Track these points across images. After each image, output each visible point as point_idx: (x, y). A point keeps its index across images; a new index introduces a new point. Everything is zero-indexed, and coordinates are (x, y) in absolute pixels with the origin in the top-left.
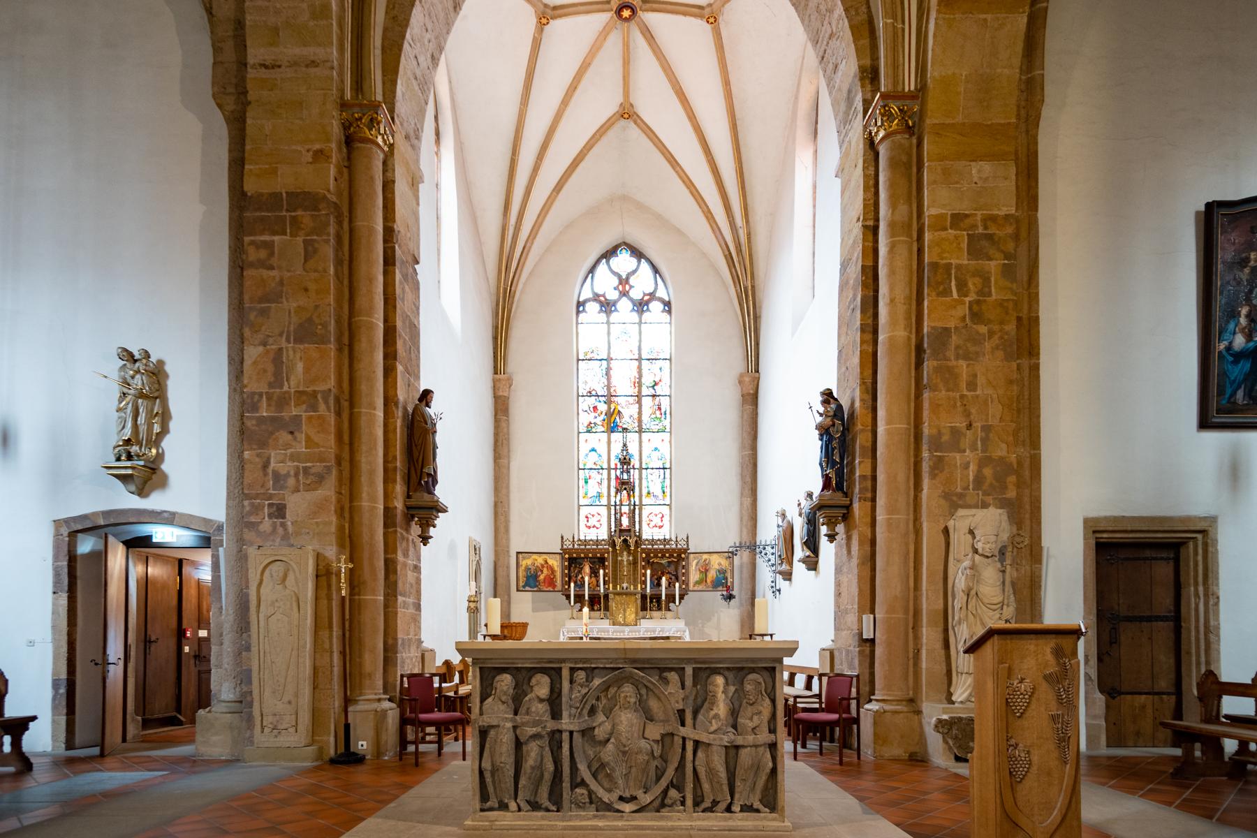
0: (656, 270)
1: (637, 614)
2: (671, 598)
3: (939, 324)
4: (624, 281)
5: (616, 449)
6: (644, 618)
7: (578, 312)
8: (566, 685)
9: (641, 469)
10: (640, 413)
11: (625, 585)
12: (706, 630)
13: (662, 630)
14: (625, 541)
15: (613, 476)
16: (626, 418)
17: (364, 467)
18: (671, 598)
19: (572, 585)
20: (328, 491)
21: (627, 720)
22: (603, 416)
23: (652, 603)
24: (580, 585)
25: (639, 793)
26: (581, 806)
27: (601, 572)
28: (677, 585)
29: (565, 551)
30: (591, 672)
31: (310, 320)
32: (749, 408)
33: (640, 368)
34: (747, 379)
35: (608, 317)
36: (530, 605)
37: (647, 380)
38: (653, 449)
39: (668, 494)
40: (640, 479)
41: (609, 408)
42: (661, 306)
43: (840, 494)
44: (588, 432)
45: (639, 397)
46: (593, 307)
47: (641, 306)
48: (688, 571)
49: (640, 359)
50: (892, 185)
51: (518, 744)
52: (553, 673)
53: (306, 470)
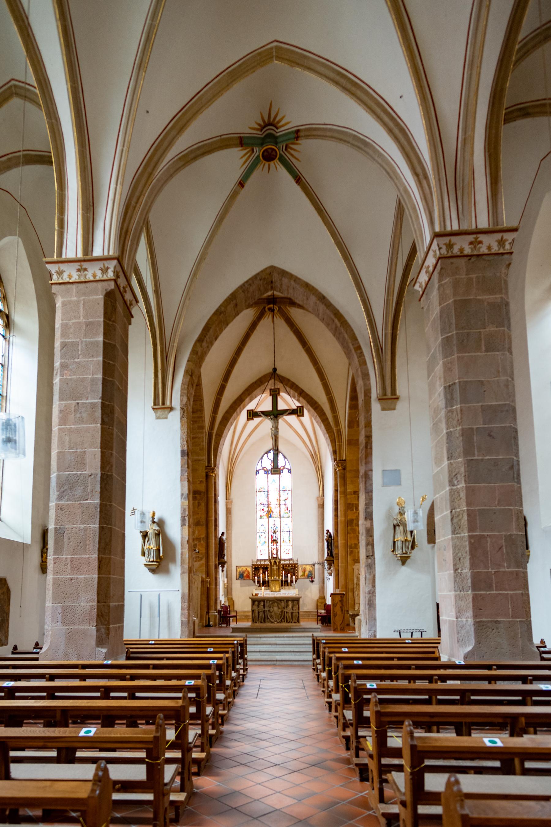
0: (285, 457)
2: (292, 581)
5: (271, 524)
7: (256, 474)
12: (306, 593)
14: (275, 561)
17: (211, 555)
18: (292, 581)
19: (256, 577)
20: (203, 561)
21: (276, 609)
22: (266, 512)
23: (285, 584)
27: (266, 573)
29: (253, 565)
30: (270, 601)
31: (199, 521)
32: (321, 509)
33: (280, 494)
34: (320, 499)
36: (239, 585)
37: (282, 499)
38: (287, 524)
46: (262, 472)
50: (340, 483)
51: (259, 613)
52: (264, 601)
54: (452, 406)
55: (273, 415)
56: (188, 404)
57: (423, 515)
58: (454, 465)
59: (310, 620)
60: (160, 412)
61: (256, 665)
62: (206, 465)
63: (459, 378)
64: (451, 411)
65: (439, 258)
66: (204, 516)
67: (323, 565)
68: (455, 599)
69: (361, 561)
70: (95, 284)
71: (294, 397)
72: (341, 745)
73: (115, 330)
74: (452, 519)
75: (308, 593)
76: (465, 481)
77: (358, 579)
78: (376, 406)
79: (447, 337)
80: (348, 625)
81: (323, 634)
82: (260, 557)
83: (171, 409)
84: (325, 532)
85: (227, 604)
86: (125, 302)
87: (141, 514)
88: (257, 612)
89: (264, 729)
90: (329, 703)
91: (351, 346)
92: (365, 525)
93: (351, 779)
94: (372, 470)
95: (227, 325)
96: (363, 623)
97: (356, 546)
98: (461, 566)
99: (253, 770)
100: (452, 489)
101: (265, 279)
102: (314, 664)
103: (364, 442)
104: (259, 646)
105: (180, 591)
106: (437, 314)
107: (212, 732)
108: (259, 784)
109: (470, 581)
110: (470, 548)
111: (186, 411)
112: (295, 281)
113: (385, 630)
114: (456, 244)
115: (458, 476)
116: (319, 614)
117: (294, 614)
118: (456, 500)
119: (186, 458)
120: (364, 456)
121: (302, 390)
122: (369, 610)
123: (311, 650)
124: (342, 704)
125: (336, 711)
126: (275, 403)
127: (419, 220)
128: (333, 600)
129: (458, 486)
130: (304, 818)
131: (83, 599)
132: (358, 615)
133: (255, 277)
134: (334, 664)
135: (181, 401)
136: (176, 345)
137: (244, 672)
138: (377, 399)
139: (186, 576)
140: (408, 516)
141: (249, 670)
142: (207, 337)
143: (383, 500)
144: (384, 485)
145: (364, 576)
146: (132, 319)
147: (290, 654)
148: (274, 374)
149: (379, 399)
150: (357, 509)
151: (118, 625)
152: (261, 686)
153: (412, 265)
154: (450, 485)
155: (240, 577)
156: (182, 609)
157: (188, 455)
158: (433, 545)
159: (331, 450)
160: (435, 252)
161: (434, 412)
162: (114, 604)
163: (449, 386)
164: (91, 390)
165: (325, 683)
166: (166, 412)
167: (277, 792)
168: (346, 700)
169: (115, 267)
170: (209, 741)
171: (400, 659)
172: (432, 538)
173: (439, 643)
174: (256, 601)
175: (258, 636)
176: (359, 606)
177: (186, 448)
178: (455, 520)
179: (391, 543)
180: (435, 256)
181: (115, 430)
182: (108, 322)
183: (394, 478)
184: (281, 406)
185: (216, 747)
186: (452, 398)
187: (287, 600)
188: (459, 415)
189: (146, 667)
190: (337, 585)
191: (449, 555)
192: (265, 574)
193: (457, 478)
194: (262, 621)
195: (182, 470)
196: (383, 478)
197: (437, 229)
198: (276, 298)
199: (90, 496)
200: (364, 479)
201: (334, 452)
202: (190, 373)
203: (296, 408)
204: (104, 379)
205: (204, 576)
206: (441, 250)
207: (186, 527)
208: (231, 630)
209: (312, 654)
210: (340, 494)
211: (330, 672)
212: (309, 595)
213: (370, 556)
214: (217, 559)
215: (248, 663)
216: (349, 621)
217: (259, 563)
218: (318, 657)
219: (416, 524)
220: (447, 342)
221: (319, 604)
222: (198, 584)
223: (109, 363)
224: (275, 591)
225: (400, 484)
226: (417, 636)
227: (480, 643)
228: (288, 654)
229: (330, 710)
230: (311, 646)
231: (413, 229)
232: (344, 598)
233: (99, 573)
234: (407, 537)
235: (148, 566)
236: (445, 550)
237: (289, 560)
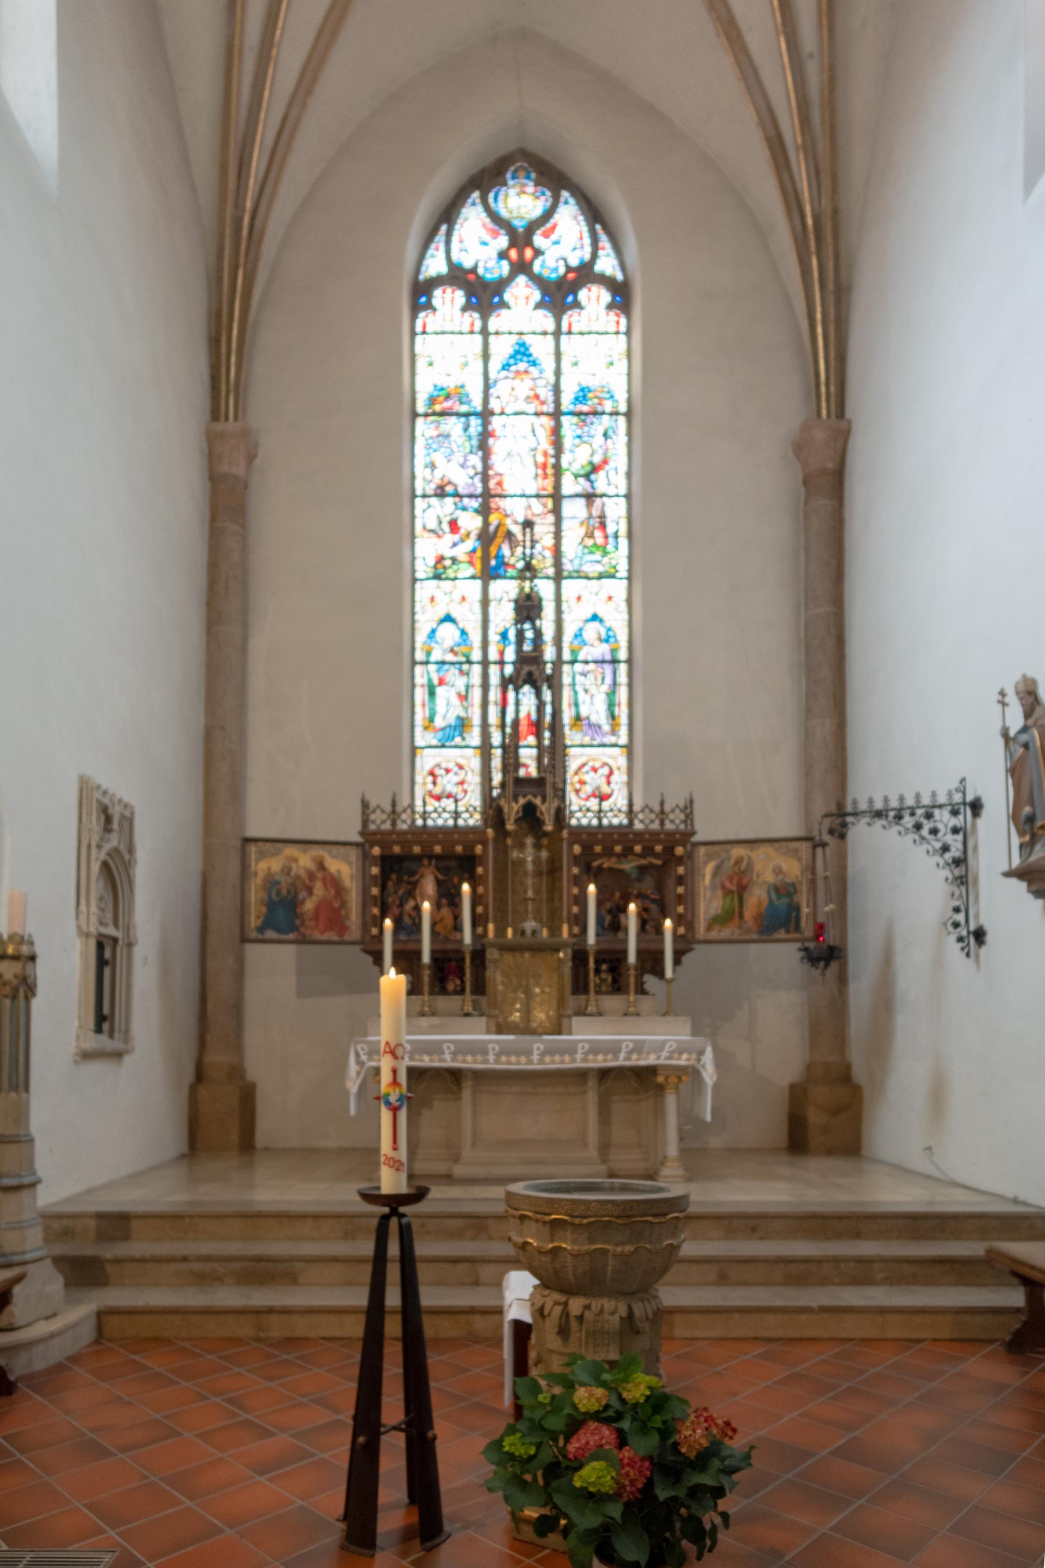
1: (561, 1003)
2: (651, 961)
4: (521, 238)
6: (581, 1013)
11: (530, 925)
14: (529, 810)
19: (388, 923)
22: (470, 544)
23: (604, 974)
27: (466, 887)
28: (668, 923)
32: (823, 503)
33: (556, 433)
37: (575, 458)
39: (624, 719)
41: (486, 523)
42: (606, 297)
44: (437, 577)
46: (449, 302)
47: (559, 295)
49: (557, 414)
155: (268, 923)
224: (525, 1029)
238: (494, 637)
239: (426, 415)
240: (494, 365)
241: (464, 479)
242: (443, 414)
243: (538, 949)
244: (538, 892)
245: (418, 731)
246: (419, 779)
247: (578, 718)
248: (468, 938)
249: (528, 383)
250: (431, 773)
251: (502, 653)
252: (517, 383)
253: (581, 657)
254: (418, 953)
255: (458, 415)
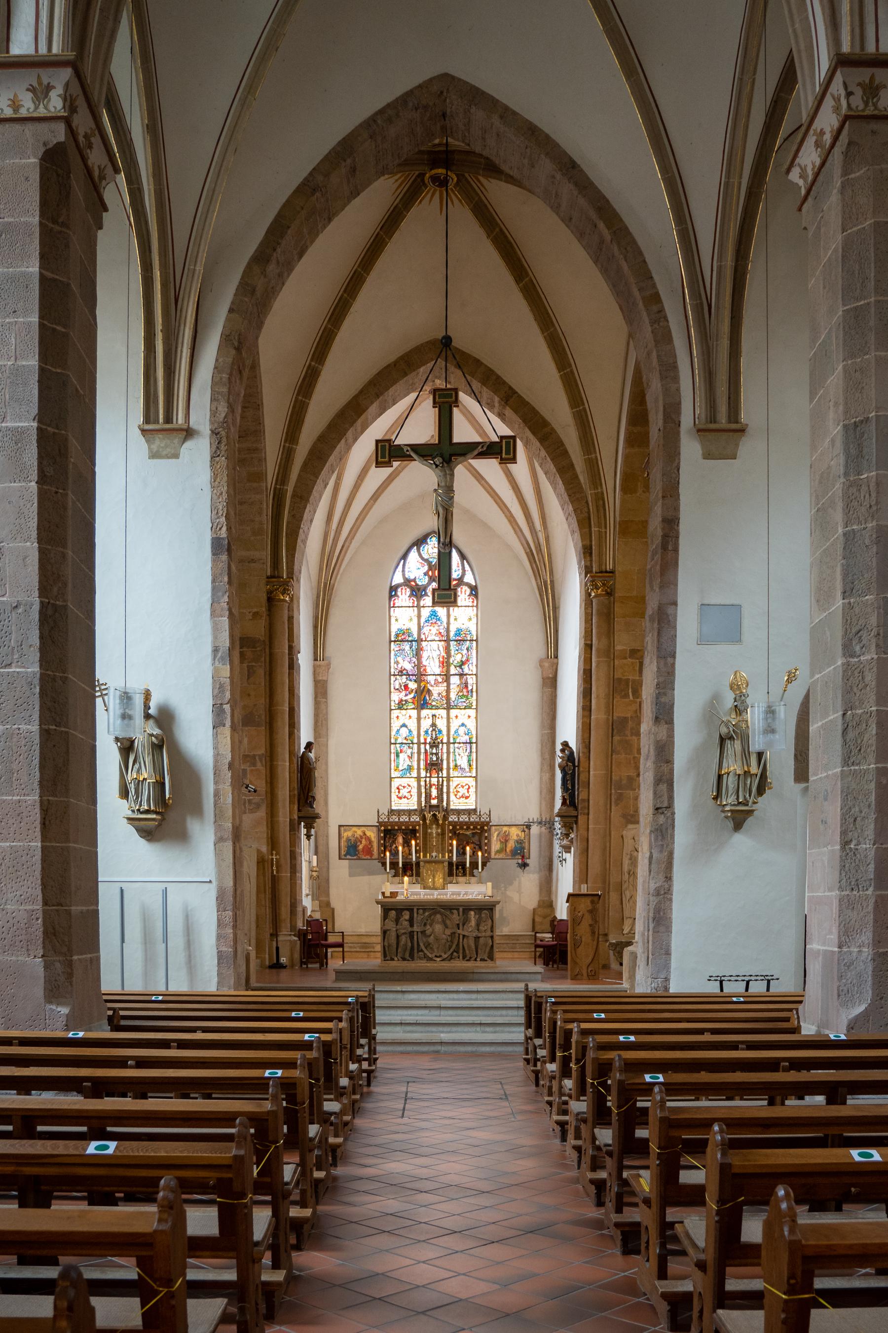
1: (444, 879)
2: (474, 865)
3: (623, 715)
5: (426, 724)
6: (451, 883)
7: (391, 597)
8: (415, 915)
9: (448, 743)
10: (448, 691)
11: (434, 854)
12: (508, 893)
13: (466, 894)
14: (434, 815)
15: (423, 750)
16: (435, 696)
19: (388, 854)
20: (262, 813)
21: (438, 928)
23: (458, 870)
24: (395, 854)
25: (443, 954)
26: (421, 959)
27: (413, 842)
29: (381, 824)
30: (424, 910)
32: (548, 690)
33: (447, 649)
34: (546, 664)
35: (418, 601)
37: (456, 658)
40: (448, 753)
41: (419, 686)
43: (572, 809)
45: (447, 677)
46: (404, 597)
48: (489, 841)
49: (448, 641)
50: (598, 627)
51: (398, 937)
52: (411, 911)
53: (249, 801)
54: (859, 473)
55: (442, 457)
56: (230, 421)
57: (787, 718)
58: (857, 610)
59: (516, 955)
60: (159, 442)
61: (394, 1053)
62: (269, 574)
63: (878, 409)
64: (857, 485)
65: (847, 118)
66: (262, 702)
67: (551, 828)
68: (840, 905)
69: (641, 819)
70: (17, 127)
71: (491, 407)
72: (587, 1199)
73: (67, 246)
74: (845, 731)
75: (512, 893)
76: (877, 646)
77: (634, 862)
78: (690, 448)
79: (856, 308)
80: (606, 967)
81: (547, 986)
82: (398, 804)
83: (188, 433)
84: (559, 747)
85: (317, 916)
86: (89, 172)
87: (121, 696)
88: (394, 934)
89: (424, 1173)
90: (562, 1125)
91: (636, 293)
92: (655, 734)
93: (605, 1252)
94: (675, 604)
95: (330, 220)
96: (641, 962)
97: (632, 783)
98: (856, 835)
99: (408, 1242)
100: (848, 664)
101: (426, 107)
102: (527, 1049)
103: (660, 533)
104: (400, 1012)
105: (215, 883)
106: (836, 250)
107: (319, 1174)
108: (424, 1262)
109: (872, 867)
110: (878, 796)
111: (224, 439)
112: (501, 117)
113: (687, 978)
114: (885, 87)
115: (864, 634)
116: (538, 942)
117: (482, 941)
118: (855, 689)
119: (224, 557)
120: (658, 567)
121: (510, 388)
122: (656, 931)
123: (522, 1020)
124: (590, 1120)
125: (578, 1136)
126: (445, 424)
127: (806, 10)
128: (572, 910)
129: (862, 658)
130: (514, 1311)
131: (10, 896)
132: (629, 944)
133: (403, 101)
134: (577, 1042)
135: (214, 413)
136: (200, 268)
137: (370, 1065)
138: (695, 430)
139: (228, 847)
140: (755, 717)
141: (379, 1063)
142: (279, 250)
143: (699, 675)
144: (703, 640)
145: (648, 855)
146: (104, 214)
147: (473, 1029)
148: (445, 347)
149: (699, 431)
150: (637, 693)
151: (89, 956)
152: (409, 1095)
153: (788, 101)
154: (844, 655)
156: (220, 924)
157: (229, 550)
158: (804, 785)
159: (580, 545)
160: (837, 100)
161: (820, 482)
162: (79, 908)
163: (856, 425)
164: (11, 398)
165: (555, 1084)
166: (176, 441)
167: (459, 1274)
168: (601, 1115)
169: (67, 86)
170: (317, 1192)
171: (714, 1032)
172: (802, 774)
173: (801, 1002)
174: (392, 909)
175: (399, 988)
176: (633, 924)
177: (224, 533)
178: (851, 735)
179: (713, 779)
180: (837, 109)
181: (71, 496)
182: (51, 225)
183: (726, 624)
184: (463, 433)
185: (324, 1204)
186: (860, 455)
187: (466, 908)
188: (874, 495)
189: (165, 1044)
190: (582, 873)
191: (833, 811)
192: (409, 846)
193: (860, 640)
194: (407, 956)
195: (214, 589)
196: (701, 623)
197: (846, 48)
198: (453, 152)
199: (16, 656)
200: (656, 625)
201: (587, 551)
202: (236, 344)
203: (497, 440)
204: (42, 370)
205: (264, 849)
206: (851, 97)
207: (227, 731)
208: (333, 976)
209: (522, 1029)
210: (598, 656)
211: (566, 1061)
212: (515, 897)
213: (664, 808)
214: (296, 807)
215: (379, 1048)
216: (608, 959)
217: (394, 818)
218: (539, 1034)
219: (771, 736)
220: (854, 321)
221: (537, 919)
222: (250, 867)
223: (54, 330)
224: (435, 888)
225: (739, 641)
226: (757, 988)
227: (881, 998)
228: (466, 1029)
229: (564, 1139)
230: (522, 1013)
231: (790, 31)
232: (600, 906)
233: (44, 838)
234: (749, 765)
235: (137, 823)
236: (826, 799)
237: (469, 812)
238: (422, 733)
239: (395, 641)
240: (423, 620)
241: (408, 667)
242: (402, 641)
243: (436, 862)
244: (438, 841)
245: (392, 771)
246: (393, 791)
247: (456, 766)
248: (414, 859)
249: (436, 627)
250: (398, 788)
251: (425, 739)
252: (432, 628)
253: (458, 741)
254: (398, 863)
255: (408, 641)
